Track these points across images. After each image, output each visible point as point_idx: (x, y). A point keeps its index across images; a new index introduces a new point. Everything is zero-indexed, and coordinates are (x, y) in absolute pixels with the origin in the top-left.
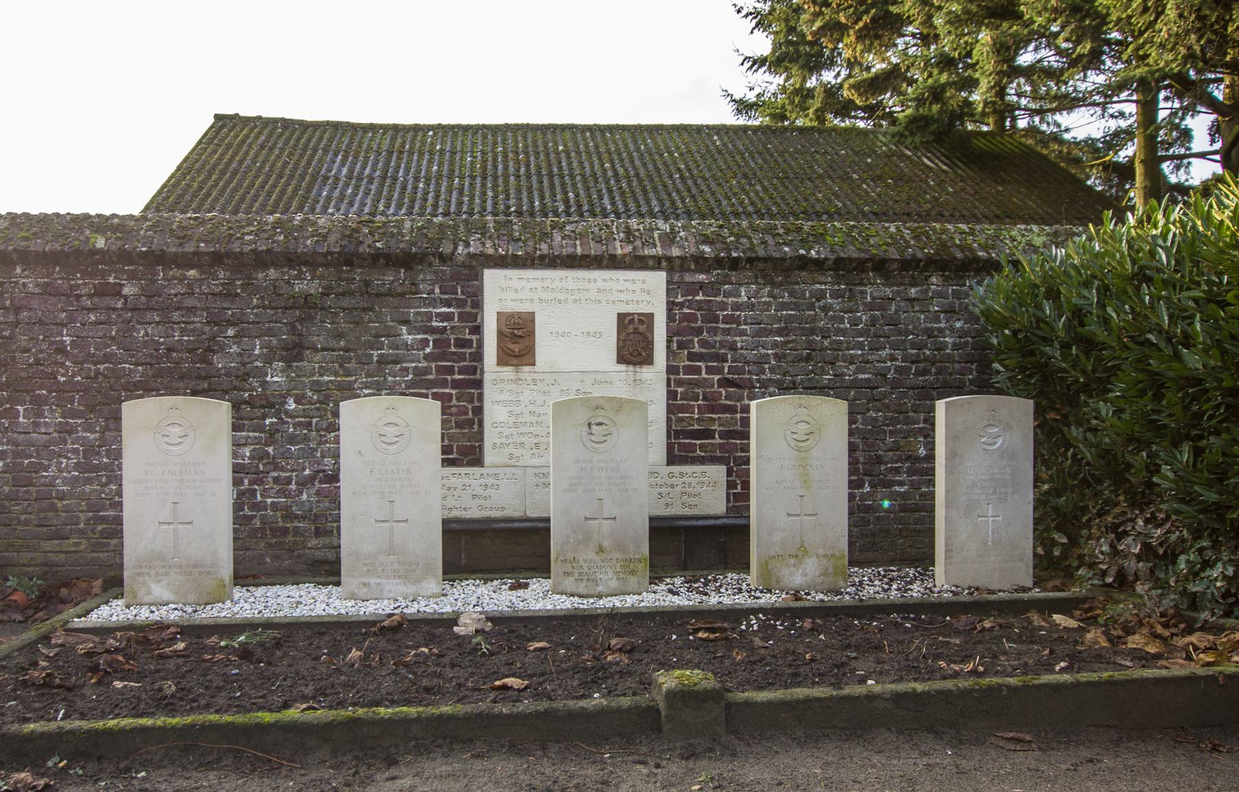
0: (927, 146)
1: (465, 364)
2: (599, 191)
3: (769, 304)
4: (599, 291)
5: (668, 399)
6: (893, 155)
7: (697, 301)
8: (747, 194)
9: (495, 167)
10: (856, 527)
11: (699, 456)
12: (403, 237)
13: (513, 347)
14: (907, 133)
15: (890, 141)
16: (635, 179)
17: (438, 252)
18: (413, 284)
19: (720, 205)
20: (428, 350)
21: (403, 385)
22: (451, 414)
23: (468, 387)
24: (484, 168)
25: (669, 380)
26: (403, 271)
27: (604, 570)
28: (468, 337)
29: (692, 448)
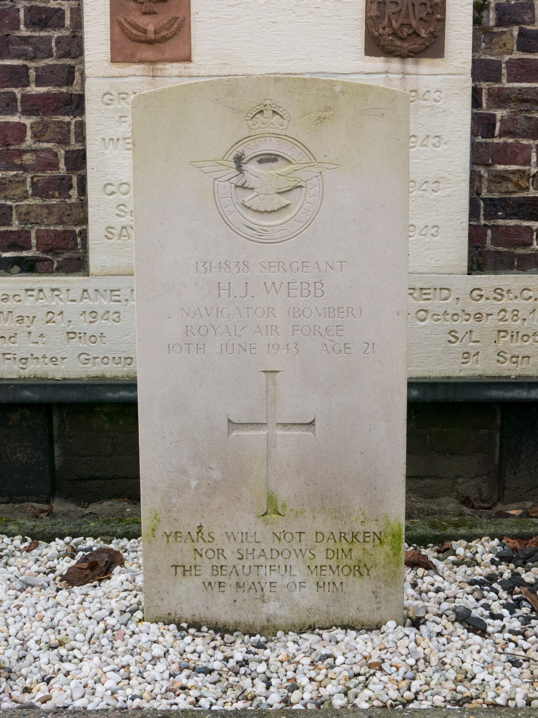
1: (50, 61)
5: (474, 134)
13: (143, 21)
22: (24, 168)
23: (56, 111)
25: (476, 94)
27: (280, 561)
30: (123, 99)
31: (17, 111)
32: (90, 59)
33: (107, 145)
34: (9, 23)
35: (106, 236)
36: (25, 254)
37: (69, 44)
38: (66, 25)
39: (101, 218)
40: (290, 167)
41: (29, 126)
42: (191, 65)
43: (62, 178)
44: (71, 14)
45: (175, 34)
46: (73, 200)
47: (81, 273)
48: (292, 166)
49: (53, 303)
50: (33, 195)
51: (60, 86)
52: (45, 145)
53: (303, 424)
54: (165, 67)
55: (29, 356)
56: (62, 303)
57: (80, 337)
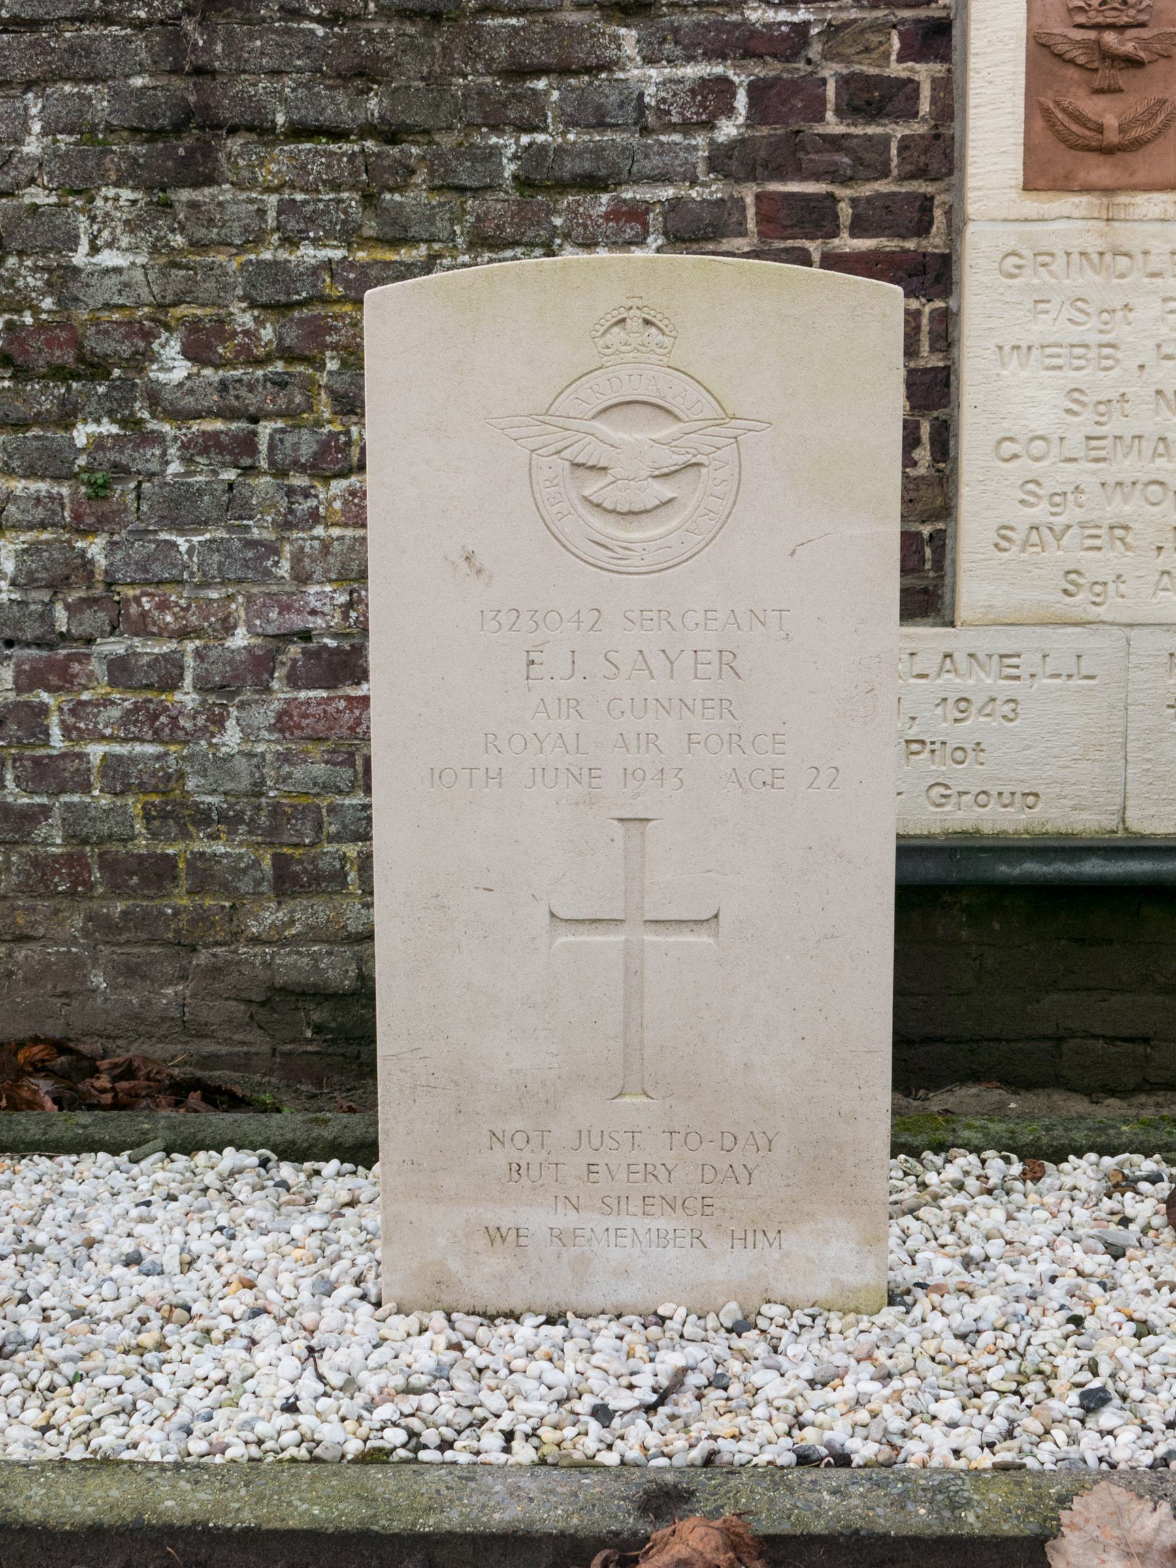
1: (883, 187)
20: (728, 130)
28: (896, 70)
30: (1044, 265)
32: (981, 184)
33: (1006, 360)
34: (804, 107)
35: (996, 545)
37: (925, 152)
38: (921, 114)
39: (988, 508)
40: (674, 428)
44: (933, 89)
45: (1159, 133)
47: (930, 620)
48: (682, 425)
51: (903, 237)
53: (583, 921)
54: (1133, 201)
57: (933, 751)
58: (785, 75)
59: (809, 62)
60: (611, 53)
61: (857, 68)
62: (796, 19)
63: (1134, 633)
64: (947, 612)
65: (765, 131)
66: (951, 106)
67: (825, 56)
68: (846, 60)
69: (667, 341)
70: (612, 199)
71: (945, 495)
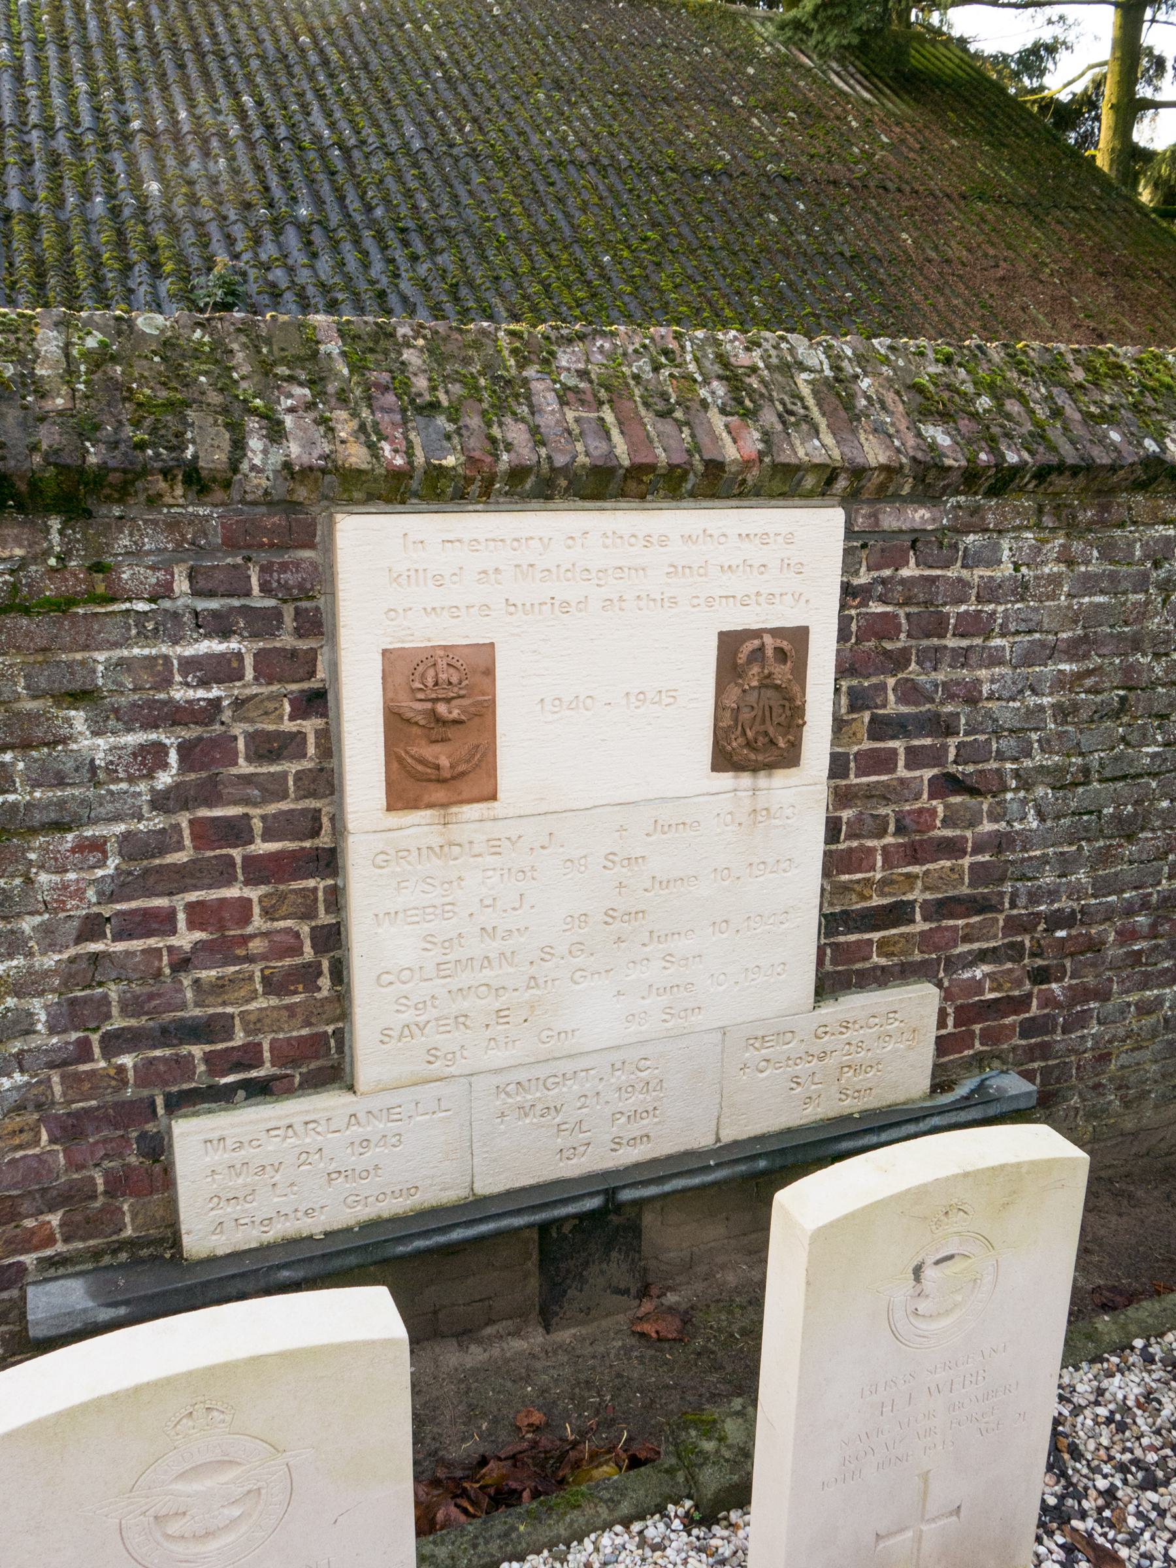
0: (844, 53)
1: (284, 806)
2: (300, 95)
3: (1055, 580)
4: (674, 570)
6: (786, 64)
7: (903, 581)
8: (568, 122)
9: (82, 23)
10: (1156, 1061)
11: (876, 967)
12: (42, 395)
13: (428, 752)
14: (813, 25)
15: (776, 37)
16: (363, 75)
17: (180, 462)
18: (98, 567)
19: (526, 142)
20: (164, 779)
21: (91, 895)
22: (249, 959)
24: (59, 24)
26: (55, 524)
28: (288, 726)
29: (861, 951)
31: (236, 880)
36: (254, 1074)
37: (314, 781)
41: (255, 900)
42: (496, 804)
43: (309, 965)
46: (325, 993)
49: (308, 1140)
50: (264, 994)
51: (301, 840)
52: (282, 924)
55: (274, 1215)
56: (320, 1138)
58: (205, 735)
59: (223, 723)
60: (63, 732)
61: (259, 726)
62: (211, 695)
63: (473, 1079)
64: (348, 1078)
65: (193, 776)
66: (330, 749)
67: (234, 719)
68: (252, 721)
69: (228, 1418)
70: (76, 837)
71: (342, 1006)
